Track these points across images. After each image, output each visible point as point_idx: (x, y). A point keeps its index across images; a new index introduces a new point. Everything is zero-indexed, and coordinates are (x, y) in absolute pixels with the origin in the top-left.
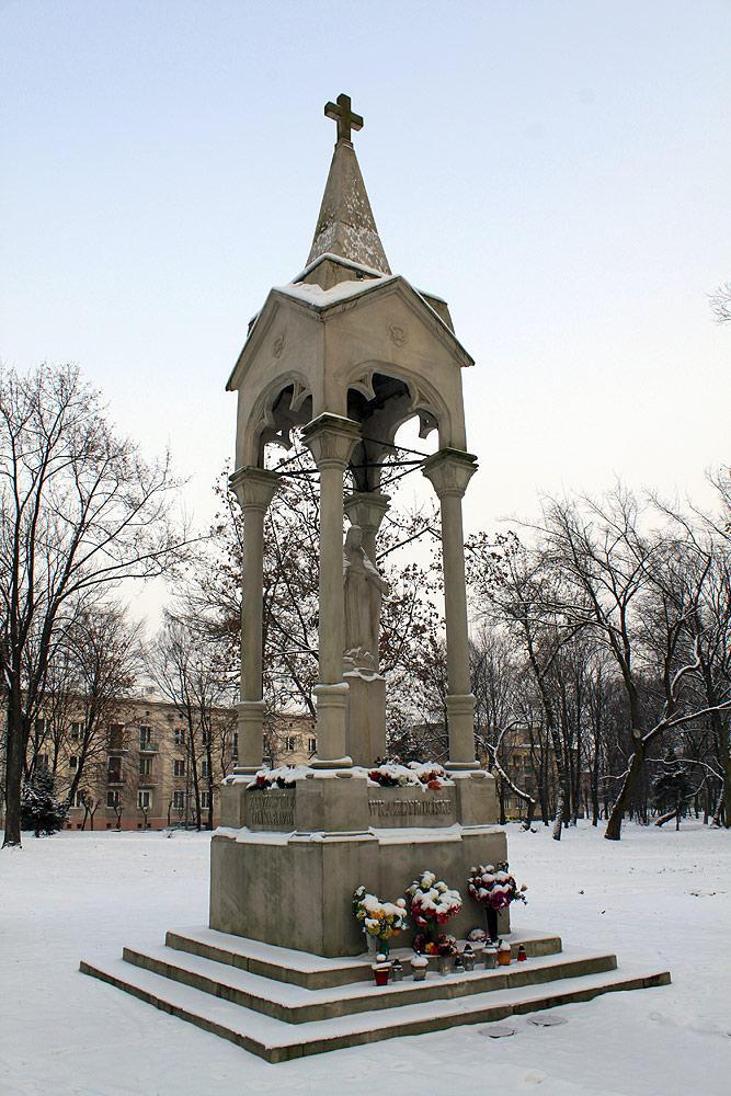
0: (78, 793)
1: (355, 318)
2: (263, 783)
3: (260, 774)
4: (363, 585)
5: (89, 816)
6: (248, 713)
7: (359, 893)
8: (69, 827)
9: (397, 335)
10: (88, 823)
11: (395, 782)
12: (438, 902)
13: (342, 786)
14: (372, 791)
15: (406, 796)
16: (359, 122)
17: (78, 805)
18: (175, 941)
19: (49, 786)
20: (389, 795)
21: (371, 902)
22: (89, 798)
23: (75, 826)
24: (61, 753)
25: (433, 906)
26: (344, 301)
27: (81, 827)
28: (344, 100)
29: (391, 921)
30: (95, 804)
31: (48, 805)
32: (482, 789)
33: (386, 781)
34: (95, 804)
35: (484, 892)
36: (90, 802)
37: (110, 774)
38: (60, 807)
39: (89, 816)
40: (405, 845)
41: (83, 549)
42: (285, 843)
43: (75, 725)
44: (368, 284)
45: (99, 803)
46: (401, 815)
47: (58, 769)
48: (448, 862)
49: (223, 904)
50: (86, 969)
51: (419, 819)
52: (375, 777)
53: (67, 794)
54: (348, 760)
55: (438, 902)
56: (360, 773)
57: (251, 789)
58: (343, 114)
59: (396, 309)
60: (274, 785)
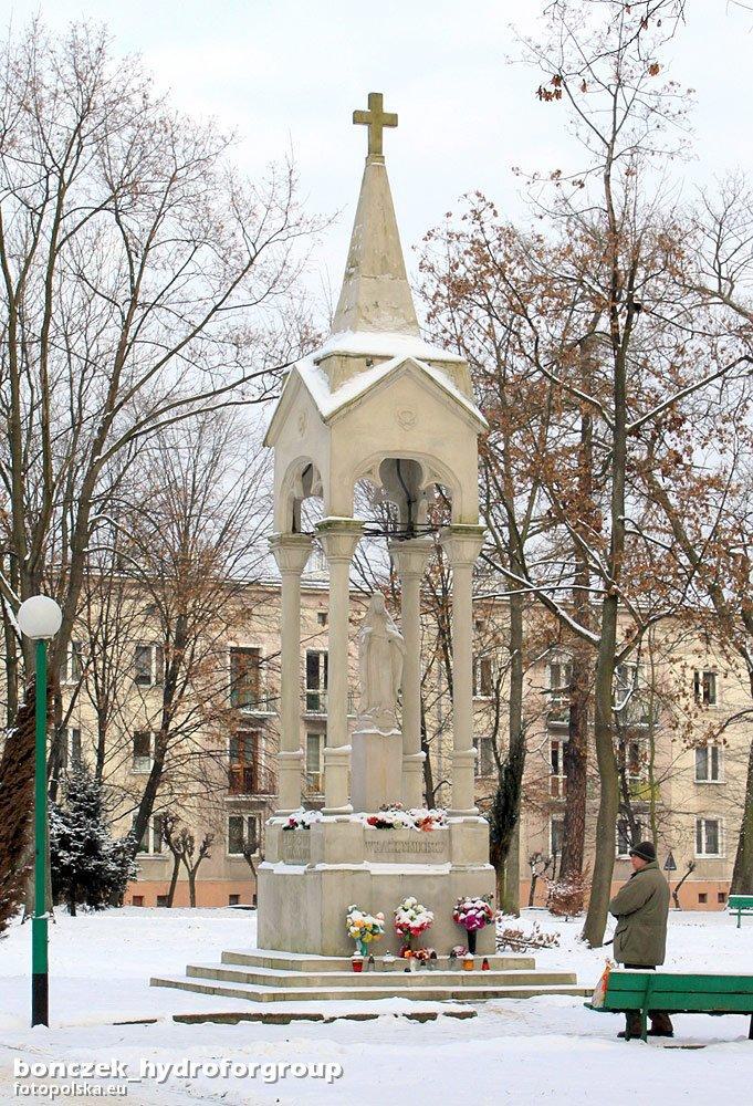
0: (157, 819)
1: (363, 415)
2: (293, 824)
3: (292, 817)
4: (385, 647)
5: (183, 875)
6: (289, 762)
7: (350, 908)
8: (138, 901)
10: (182, 891)
11: (390, 826)
12: (412, 919)
13: (341, 828)
15: (400, 836)
16: (392, 121)
17: (157, 850)
18: (229, 957)
19: (90, 807)
20: (384, 834)
21: (356, 916)
22: (184, 832)
23: (151, 897)
24: (112, 731)
25: (408, 921)
26: (347, 404)
27: (165, 901)
28: (375, 99)
29: (370, 929)
30: (198, 845)
31: (92, 847)
32: (475, 833)
33: (381, 825)
34: (198, 845)
35: (463, 916)
36: (187, 841)
37: (231, 774)
38: (118, 851)
39: (183, 875)
40: (394, 876)
41: (141, 356)
42: (302, 873)
44: (381, 370)
45: (206, 844)
46: (396, 852)
47: (107, 769)
48: (435, 891)
49: (266, 926)
50: (156, 983)
51: (413, 856)
52: (372, 821)
53: (128, 823)
54: (350, 807)
55: (412, 919)
56: (361, 819)
57: (286, 829)
58: (375, 117)
59: (406, 390)
60: (300, 826)
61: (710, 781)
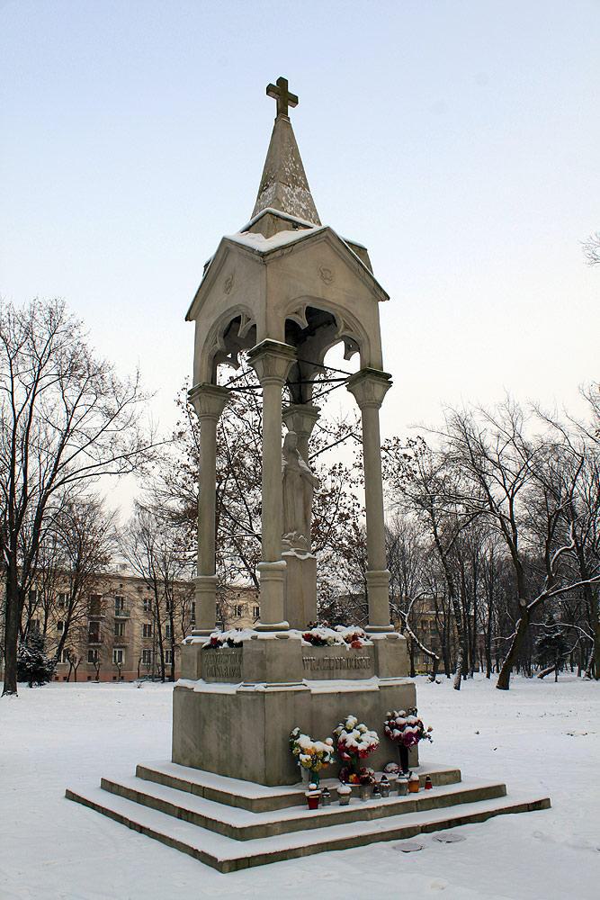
0: (64, 651)
1: (291, 261)
2: (215, 643)
3: (213, 635)
4: (298, 480)
5: (73, 670)
6: (203, 585)
7: (295, 733)
8: (57, 679)
10: (72, 675)
11: (324, 642)
12: (359, 741)
13: (281, 645)
14: (305, 650)
15: (333, 654)
16: (294, 100)
17: (64, 661)
18: (143, 773)
19: (40, 645)
20: (319, 653)
21: (304, 741)
22: (73, 656)
23: (61, 678)
24: (50, 618)
25: (355, 744)
26: (282, 248)
28: (282, 82)
29: (321, 756)
30: (78, 660)
31: (40, 661)
32: (396, 648)
33: (317, 642)
34: (78, 660)
35: (397, 732)
36: (74, 659)
37: (90, 636)
38: (49, 663)
39: (73, 670)
40: (333, 694)
42: (234, 692)
43: (62, 595)
44: (302, 233)
45: (81, 659)
46: (329, 669)
47: (48, 632)
48: (367, 708)
49: (183, 742)
50: (71, 796)
51: (344, 673)
52: (308, 638)
53: (55, 652)
54: (286, 624)
55: (359, 741)
56: (296, 635)
57: (206, 648)
58: (282, 94)
59: (325, 254)
60: (225, 645)
61: (117, 650)
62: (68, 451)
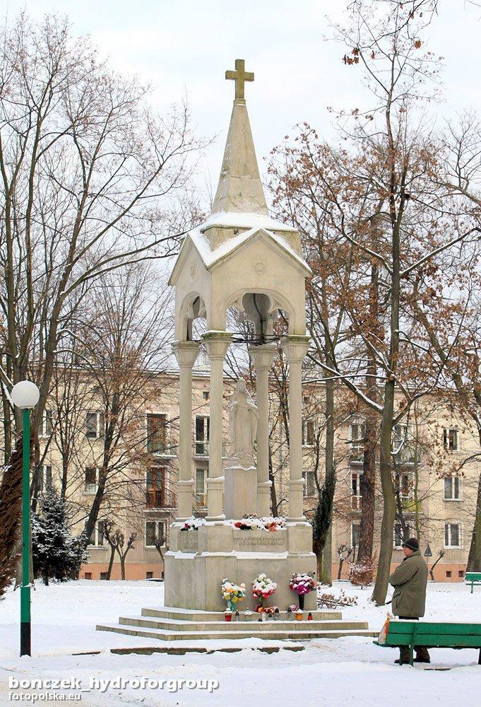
0: (100, 524)
1: (232, 266)
2: (187, 527)
3: (186, 522)
4: (246, 413)
5: (117, 559)
6: (185, 487)
7: (224, 581)
8: (88, 576)
9: (259, 269)
10: (116, 570)
11: (249, 528)
12: (263, 587)
13: (218, 529)
14: (236, 532)
15: (255, 534)
16: (251, 77)
17: (101, 543)
18: (146, 612)
19: (57, 516)
20: (245, 533)
21: (228, 586)
22: (118, 532)
23: (96, 574)
24: (72, 468)
25: (261, 589)
26: (222, 259)
28: (240, 63)
29: (236, 594)
30: (126, 540)
31: (59, 541)
32: (303, 532)
33: (244, 527)
34: (126, 540)
35: (295, 586)
36: (120, 538)
37: (148, 495)
38: (75, 544)
39: (117, 559)
40: (252, 560)
42: (193, 558)
43: (91, 415)
44: (243, 236)
45: (132, 539)
46: (253, 545)
47: (69, 491)
48: (278, 570)
49: (170, 592)
50: (100, 628)
51: (264, 547)
52: (238, 525)
53: (82, 526)
54: (223, 516)
55: (263, 587)
56: (230, 523)
57: (182, 530)
58: (240, 75)
59: (259, 249)
60: (192, 528)
62: (90, 227)
